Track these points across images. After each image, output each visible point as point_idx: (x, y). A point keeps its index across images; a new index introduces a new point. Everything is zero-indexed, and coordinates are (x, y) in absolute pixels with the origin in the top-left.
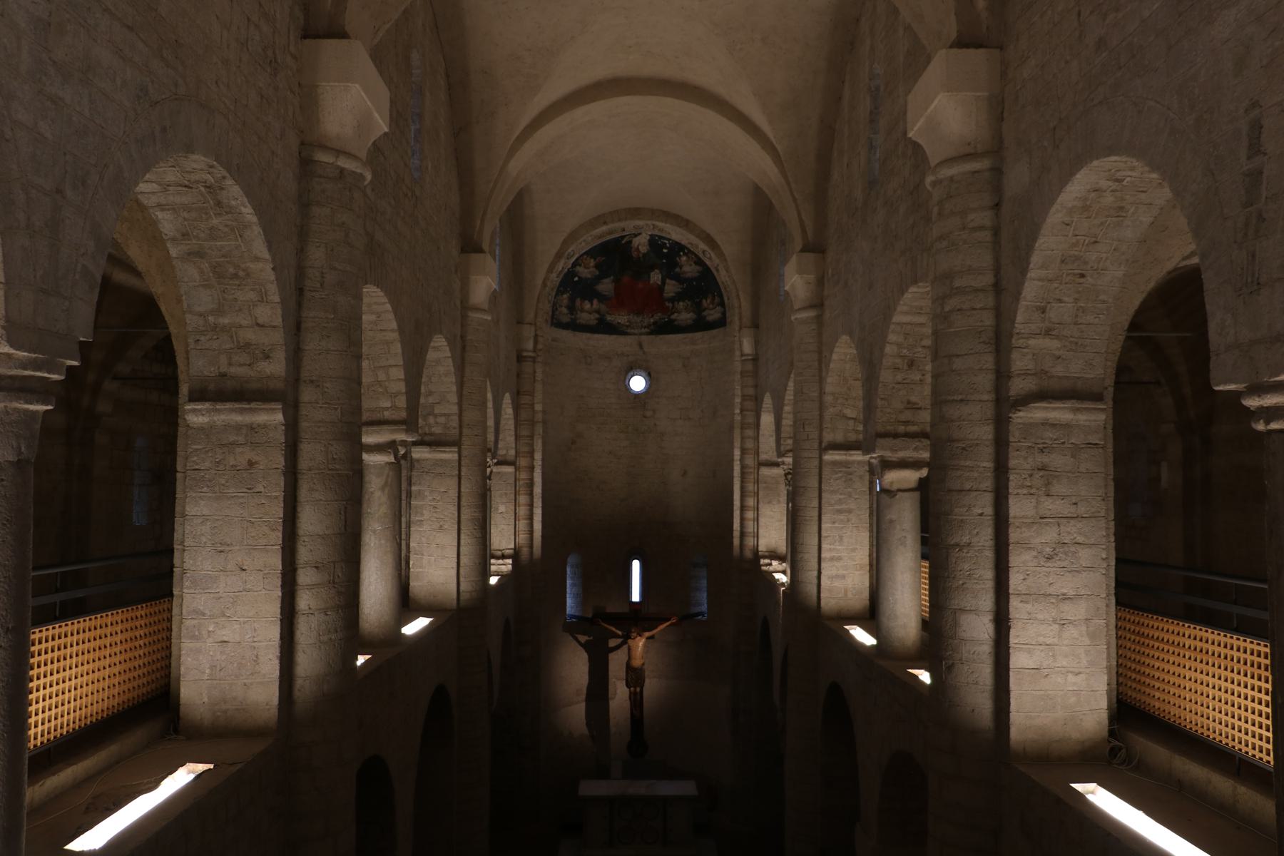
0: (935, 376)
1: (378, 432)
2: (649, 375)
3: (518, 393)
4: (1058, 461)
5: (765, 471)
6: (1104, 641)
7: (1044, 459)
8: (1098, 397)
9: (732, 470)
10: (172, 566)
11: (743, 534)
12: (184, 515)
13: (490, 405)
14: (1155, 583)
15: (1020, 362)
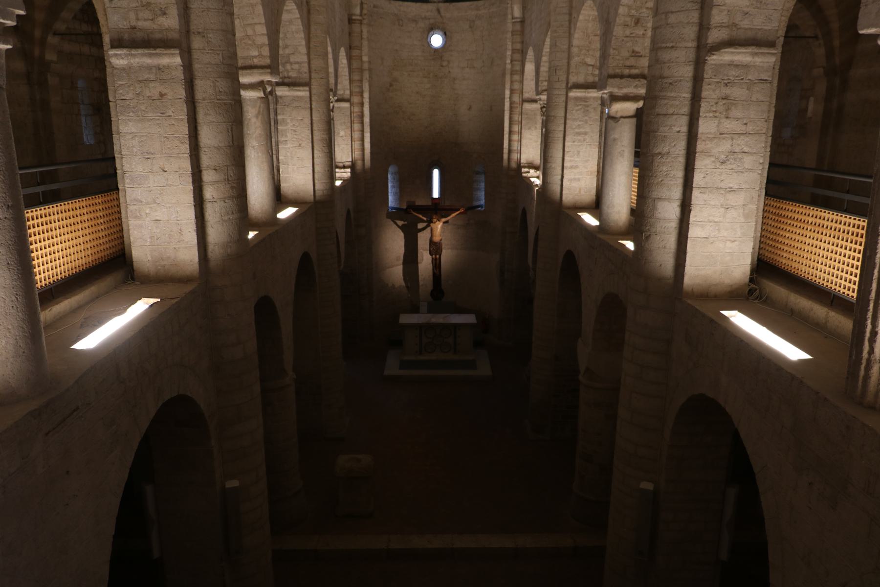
0: (655, 29)
1: (250, 75)
2: (445, 34)
3: (350, 47)
4: (737, 92)
5: (527, 106)
6: (754, 219)
7: (727, 91)
8: (771, 44)
9: (504, 105)
10: (115, 169)
11: (510, 151)
12: (119, 133)
13: (330, 56)
14: (792, 181)
15: (717, 17)
